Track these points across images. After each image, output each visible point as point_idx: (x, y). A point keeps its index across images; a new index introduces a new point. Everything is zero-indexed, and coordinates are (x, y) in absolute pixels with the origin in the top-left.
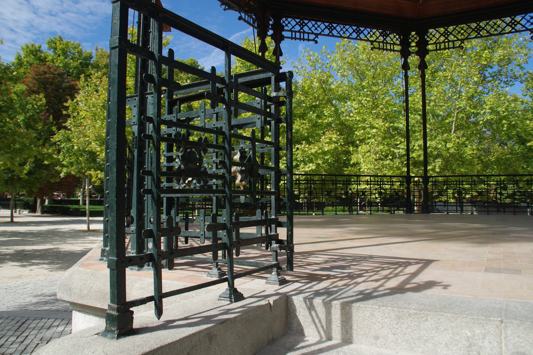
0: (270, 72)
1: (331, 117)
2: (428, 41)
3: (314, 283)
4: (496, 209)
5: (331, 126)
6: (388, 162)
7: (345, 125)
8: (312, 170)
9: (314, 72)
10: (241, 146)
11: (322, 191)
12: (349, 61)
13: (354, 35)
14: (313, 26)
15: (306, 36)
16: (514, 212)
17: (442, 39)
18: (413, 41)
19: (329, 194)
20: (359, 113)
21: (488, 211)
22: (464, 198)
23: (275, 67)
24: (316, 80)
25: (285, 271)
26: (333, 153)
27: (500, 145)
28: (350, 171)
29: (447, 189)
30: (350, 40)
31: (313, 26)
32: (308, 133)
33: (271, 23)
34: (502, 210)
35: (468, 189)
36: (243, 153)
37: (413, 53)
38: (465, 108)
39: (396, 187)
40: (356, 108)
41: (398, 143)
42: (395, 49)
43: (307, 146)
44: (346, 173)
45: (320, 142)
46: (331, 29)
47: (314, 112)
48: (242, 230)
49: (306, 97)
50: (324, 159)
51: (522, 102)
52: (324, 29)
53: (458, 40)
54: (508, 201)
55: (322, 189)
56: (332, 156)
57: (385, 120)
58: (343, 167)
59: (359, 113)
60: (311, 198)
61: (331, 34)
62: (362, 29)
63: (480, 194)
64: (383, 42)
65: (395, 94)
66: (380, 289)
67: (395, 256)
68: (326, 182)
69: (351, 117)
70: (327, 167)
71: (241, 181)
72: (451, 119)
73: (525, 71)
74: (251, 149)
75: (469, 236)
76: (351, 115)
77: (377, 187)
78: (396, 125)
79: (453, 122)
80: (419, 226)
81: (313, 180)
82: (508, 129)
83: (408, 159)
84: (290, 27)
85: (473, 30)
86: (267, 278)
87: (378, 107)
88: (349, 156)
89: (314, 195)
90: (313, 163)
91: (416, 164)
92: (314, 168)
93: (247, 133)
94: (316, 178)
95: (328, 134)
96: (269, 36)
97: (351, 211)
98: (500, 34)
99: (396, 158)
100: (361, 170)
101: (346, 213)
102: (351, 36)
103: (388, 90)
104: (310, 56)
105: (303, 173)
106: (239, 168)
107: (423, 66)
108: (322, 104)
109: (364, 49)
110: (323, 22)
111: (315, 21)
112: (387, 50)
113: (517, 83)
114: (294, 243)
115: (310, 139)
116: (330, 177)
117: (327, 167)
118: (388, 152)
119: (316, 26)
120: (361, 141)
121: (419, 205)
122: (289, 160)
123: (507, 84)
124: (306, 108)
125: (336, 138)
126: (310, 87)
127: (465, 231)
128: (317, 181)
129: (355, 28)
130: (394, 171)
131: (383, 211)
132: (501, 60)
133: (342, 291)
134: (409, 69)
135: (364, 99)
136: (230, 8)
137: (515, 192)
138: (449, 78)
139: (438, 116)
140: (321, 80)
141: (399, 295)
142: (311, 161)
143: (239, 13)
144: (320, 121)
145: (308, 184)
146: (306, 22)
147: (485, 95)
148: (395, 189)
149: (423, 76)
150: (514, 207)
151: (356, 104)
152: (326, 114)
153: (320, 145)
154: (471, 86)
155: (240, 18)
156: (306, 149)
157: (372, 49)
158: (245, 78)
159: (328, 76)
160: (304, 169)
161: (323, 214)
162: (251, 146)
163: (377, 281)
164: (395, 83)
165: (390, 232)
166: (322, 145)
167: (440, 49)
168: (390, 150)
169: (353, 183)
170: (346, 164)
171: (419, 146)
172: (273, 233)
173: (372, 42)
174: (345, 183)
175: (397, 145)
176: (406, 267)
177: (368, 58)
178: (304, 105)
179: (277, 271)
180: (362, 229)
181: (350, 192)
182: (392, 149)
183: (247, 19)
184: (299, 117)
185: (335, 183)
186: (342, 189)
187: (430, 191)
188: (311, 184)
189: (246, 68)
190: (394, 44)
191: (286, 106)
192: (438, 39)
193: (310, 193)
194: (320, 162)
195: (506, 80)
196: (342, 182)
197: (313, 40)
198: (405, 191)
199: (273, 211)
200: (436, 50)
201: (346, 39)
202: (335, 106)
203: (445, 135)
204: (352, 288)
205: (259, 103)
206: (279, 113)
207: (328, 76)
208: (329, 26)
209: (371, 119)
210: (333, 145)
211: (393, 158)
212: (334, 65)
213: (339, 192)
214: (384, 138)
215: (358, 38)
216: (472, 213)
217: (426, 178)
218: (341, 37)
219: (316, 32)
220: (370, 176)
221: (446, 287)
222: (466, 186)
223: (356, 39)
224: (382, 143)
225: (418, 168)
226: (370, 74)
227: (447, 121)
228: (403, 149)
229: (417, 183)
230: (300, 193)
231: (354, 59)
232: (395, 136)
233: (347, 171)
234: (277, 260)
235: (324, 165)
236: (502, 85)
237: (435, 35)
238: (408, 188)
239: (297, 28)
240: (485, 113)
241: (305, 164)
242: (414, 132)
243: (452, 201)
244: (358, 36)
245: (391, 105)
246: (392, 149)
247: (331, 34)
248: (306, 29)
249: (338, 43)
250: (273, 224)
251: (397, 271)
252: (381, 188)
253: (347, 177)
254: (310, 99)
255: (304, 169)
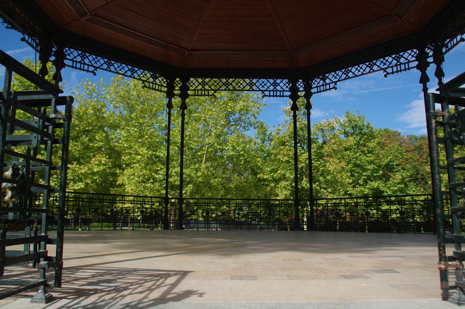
0: (51, 94)
1: (102, 142)
2: (299, 88)
3: (81, 298)
4: (235, 226)
5: (101, 150)
6: (149, 185)
7: (114, 149)
8: (81, 188)
9: (90, 100)
10: (14, 162)
11: (89, 208)
12: (122, 95)
13: (129, 73)
14: (94, 59)
15: (86, 67)
16: (248, 228)
17: (200, 87)
18: (177, 85)
19: (96, 211)
20: (127, 141)
21: (229, 228)
22: (211, 217)
23: (56, 90)
24: (91, 107)
25: (52, 288)
26: (101, 174)
27: (238, 175)
28: (116, 191)
29: (197, 209)
30: (124, 77)
31: (94, 59)
32: (80, 154)
33: (54, 50)
34: (239, 227)
35: (214, 210)
36: (16, 170)
37: (176, 95)
38: (214, 144)
39: (155, 207)
40: (124, 136)
41: (159, 169)
42: (162, 90)
43: (78, 166)
44: (112, 192)
45: (90, 163)
46: (109, 65)
47: (87, 136)
48: (8, 248)
49: (80, 122)
50: (93, 179)
51: (255, 144)
52: (103, 64)
53: (212, 90)
54: (243, 219)
55: (90, 206)
56: (100, 177)
57: (149, 148)
58: (110, 187)
59: (127, 141)
60: (78, 214)
61: (108, 69)
62: (136, 69)
63: (223, 213)
64: (152, 83)
65: (159, 127)
66: (145, 300)
67: (157, 269)
68: (94, 200)
69: (120, 143)
70: (95, 187)
71: (11, 198)
72: (202, 152)
73: (257, 120)
74: (24, 166)
75: (216, 249)
76: (120, 141)
77: (139, 206)
78: (157, 154)
79: (204, 154)
80: (175, 241)
81: (82, 198)
82: (245, 163)
83: (167, 183)
84: (72, 57)
85: (224, 84)
86: (33, 296)
87: (144, 136)
88: (116, 177)
89: (82, 212)
90: (82, 182)
91: (173, 187)
92: (83, 186)
93: (19, 150)
94: (84, 196)
95: (98, 157)
96: (51, 61)
97: (115, 227)
98: (242, 90)
99: (156, 181)
100: (126, 191)
101: (111, 228)
102: (126, 74)
103: (153, 123)
104: (88, 85)
105: (72, 191)
106: (10, 185)
107: (184, 107)
108: (94, 129)
109: (135, 86)
110: (103, 58)
111: (95, 55)
112: (155, 90)
113: (252, 129)
114: (63, 258)
115: (81, 160)
116: (97, 195)
117: (95, 187)
118: (150, 176)
119: (96, 60)
120: (128, 165)
121: (175, 223)
122: (63, 179)
123: (245, 128)
124: (80, 132)
125: (105, 161)
126: (85, 113)
127: (212, 245)
128: (85, 199)
129: (130, 67)
130: (154, 192)
131: (144, 227)
132: (241, 110)
133: (110, 305)
134: (172, 108)
135: (132, 129)
136: (13, 27)
137: (248, 212)
138: (203, 119)
139: (192, 149)
140: (95, 108)
141: (162, 305)
142: (81, 180)
143: (23, 34)
144: (91, 144)
145: (76, 201)
146: (87, 55)
147: (229, 135)
148: (155, 209)
149: (183, 115)
150: (248, 224)
151: (124, 133)
152: (97, 138)
153: (90, 166)
154: (219, 127)
155: (23, 39)
156: (77, 169)
157: (143, 87)
158: (24, 97)
159: (102, 105)
160: (73, 188)
161: (89, 230)
162: (25, 163)
163: (141, 292)
164: (160, 118)
165: (151, 247)
166: (92, 166)
167: (198, 95)
168: (151, 174)
169: (118, 202)
170: (113, 184)
171: (175, 172)
172: (41, 251)
173: (144, 82)
174: (111, 201)
175: (158, 170)
176: (166, 278)
177: (138, 94)
178: (77, 128)
179: (44, 289)
180: (128, 244)
181: (115, 210)
182: (153, 174)
183: (30, 41)
184: (73, 139)
185: (101, 201)
186: (108, 207)
187: (184, 210)
188: (79, 201)
189: (24, 87)
190: (162, 86)
191: (64, 128)
192: (197, 87)
193: (78, 210)
194: (89, 181)
195: (244, 125)
196: (108, 201)
197: (92, 72)
198: (164, 210)
199: (44, 228)
200: (195, 95)
201: (121, 76)
202: (106, 133)
203: (197, 165)
204: (119, 301)
205: (36, 123)
206: (57, 133)
207: (102, 105)
208: (107, 62)
209: (137, 147)
210: (102, 167)
211: (153, 182)
212: (108, 97)
213: (105, 209)
214: (147, 164)
215: (132, 76)
216: (217, 230)
217: (181, 200)
218: (118, 73)
219: (95, 65)
220: (134, 196)
221: (201, 295)
222: (212, 207)
223: (130, 76)
224: (145, 168)
225: (175, 191)
226: (139, 108)
227: (199, 153)
228: (162, 175)
229: (173, 204)
230: (68, 210)
231: (126, 93)
232: (157, 163)
233: (113, 191)
234: (44, 277)
235: (92, 185)
236: (241, 129)
237: (194, 83)
238: (166, 208)
239: (79, 59)
240: (228, 149)
241: (75, 183)
242: (173, 160)
243: (201, 219)
244: (132, 74)
245: (155, 136)
246: (153, 174)
247: (108, 69)
248: (86, 61)
249: (113, 78)
250: (43, 241)
251: (158, 283)
252: (143, 207)
253: (112, 197)
254: (84, 124)
255: (73, 188)
